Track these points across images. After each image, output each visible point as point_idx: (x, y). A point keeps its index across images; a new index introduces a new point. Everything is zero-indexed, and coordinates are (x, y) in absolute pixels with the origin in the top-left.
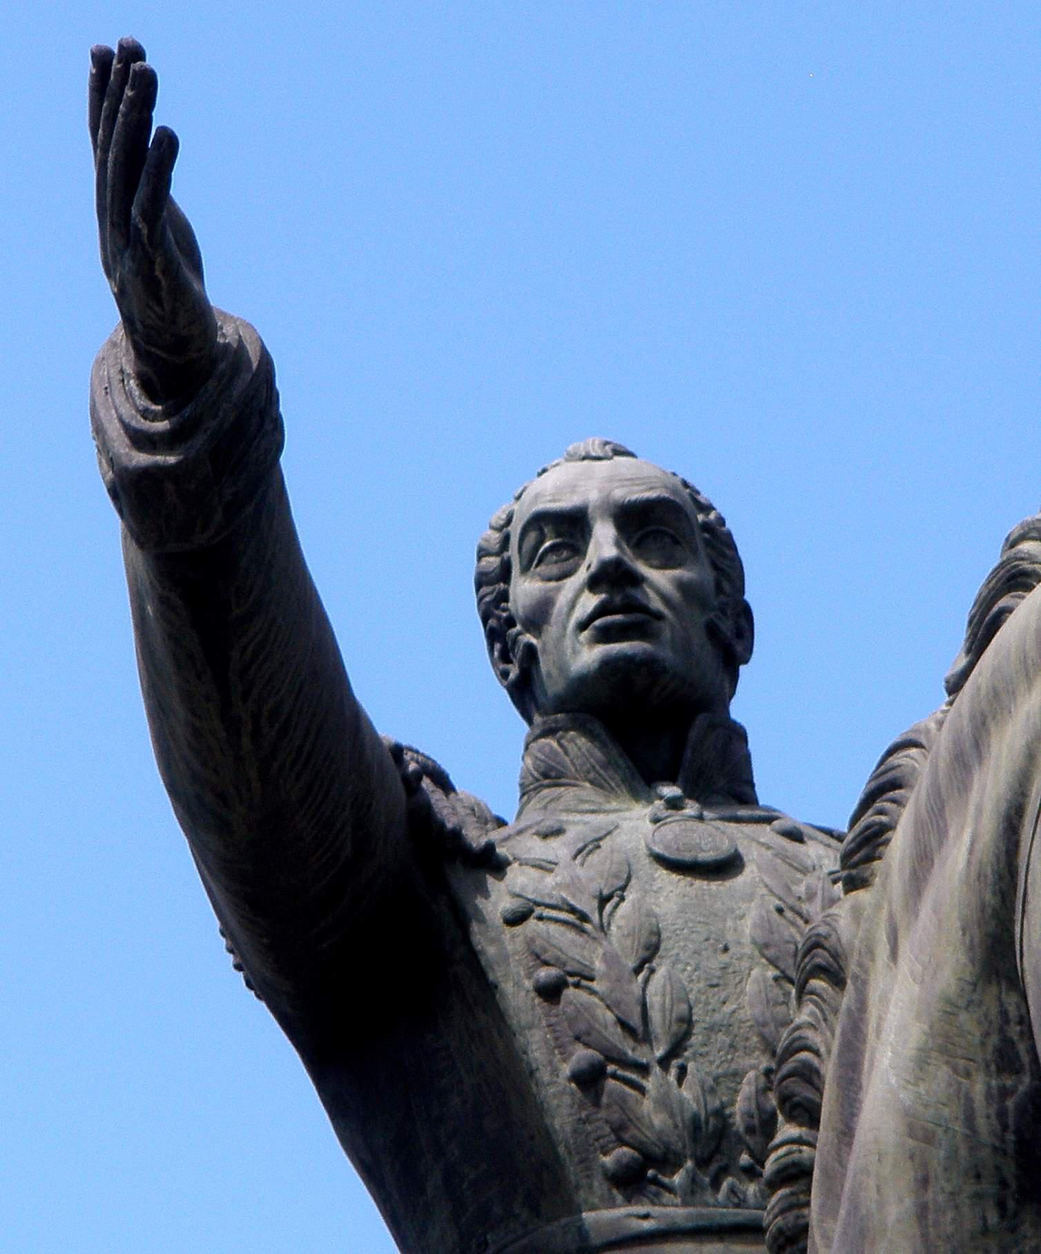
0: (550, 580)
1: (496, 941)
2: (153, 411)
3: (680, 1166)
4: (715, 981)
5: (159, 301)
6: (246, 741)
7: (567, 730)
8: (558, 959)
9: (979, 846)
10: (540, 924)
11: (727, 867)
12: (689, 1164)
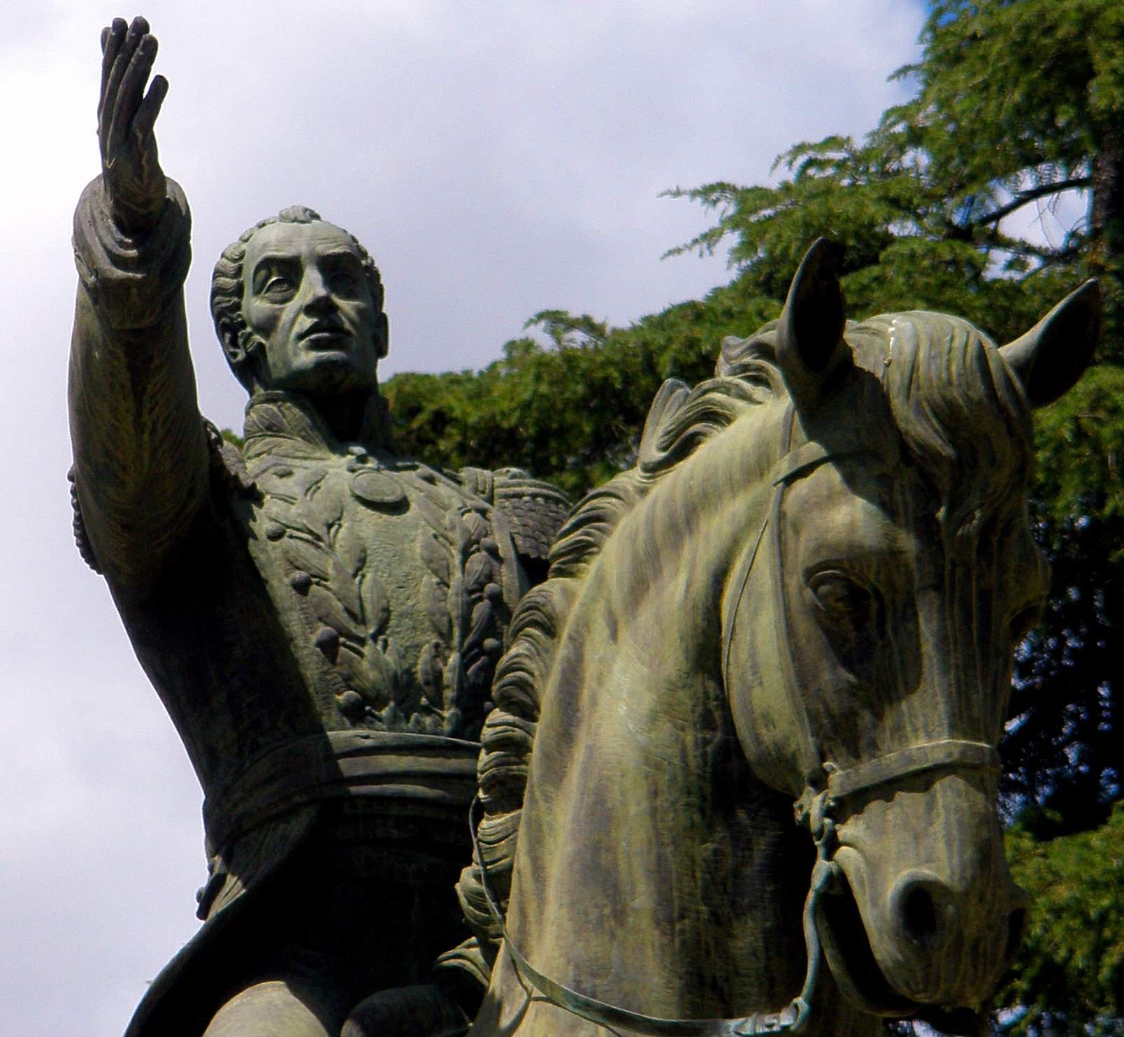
0: (276, 303)
1: (264, 551)
2: (126, 243)
3: (386, 705)
4: (402, 584)
5: (140, 177)
6: (146, 436)
7: (284, 401)
8: (305, 566)
9: (694, 589)
10: (292, 541)
11: (399, 507)
12: (392, 704)
